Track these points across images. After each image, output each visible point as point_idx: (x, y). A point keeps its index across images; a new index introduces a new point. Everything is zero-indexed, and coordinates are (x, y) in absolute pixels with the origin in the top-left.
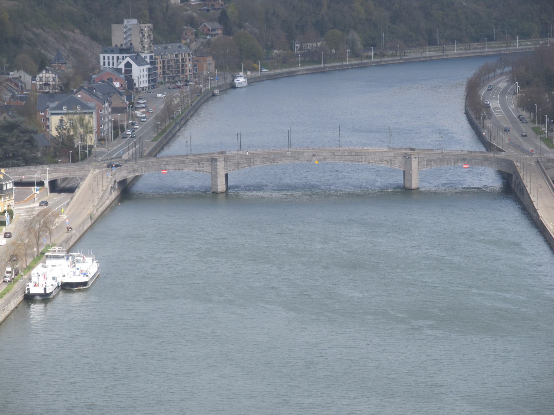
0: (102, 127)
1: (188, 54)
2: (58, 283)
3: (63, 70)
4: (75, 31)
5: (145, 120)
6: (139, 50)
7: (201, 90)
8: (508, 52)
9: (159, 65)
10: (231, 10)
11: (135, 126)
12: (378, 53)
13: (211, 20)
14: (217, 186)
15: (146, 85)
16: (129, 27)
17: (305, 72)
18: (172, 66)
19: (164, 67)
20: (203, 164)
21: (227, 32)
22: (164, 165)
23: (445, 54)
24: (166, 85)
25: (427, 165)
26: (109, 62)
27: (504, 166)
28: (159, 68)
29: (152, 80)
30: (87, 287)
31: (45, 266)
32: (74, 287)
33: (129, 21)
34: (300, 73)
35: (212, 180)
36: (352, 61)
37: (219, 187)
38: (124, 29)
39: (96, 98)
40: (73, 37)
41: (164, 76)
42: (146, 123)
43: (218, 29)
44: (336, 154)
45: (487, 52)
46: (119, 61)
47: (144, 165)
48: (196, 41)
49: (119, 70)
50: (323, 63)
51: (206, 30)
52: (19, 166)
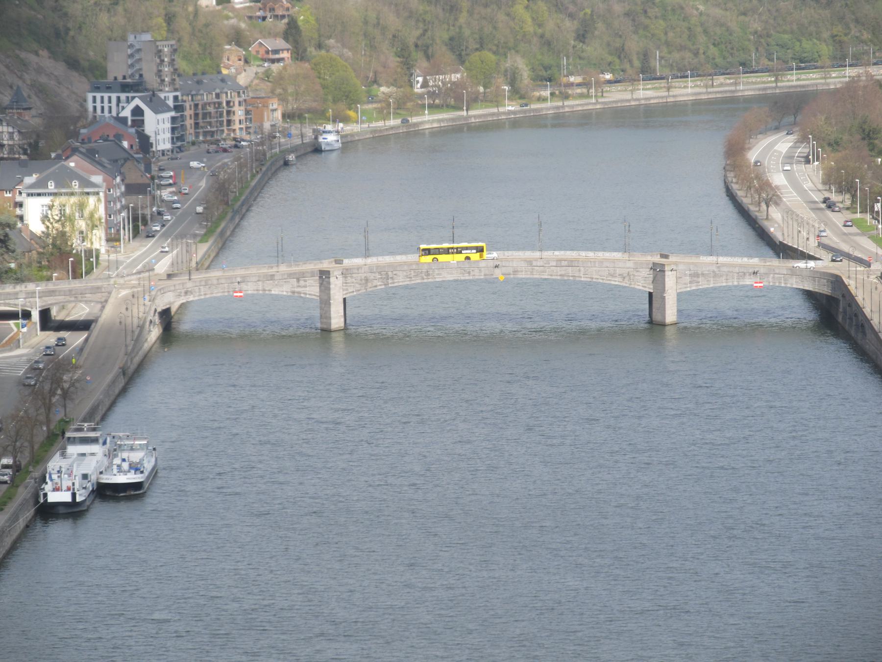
0: (112, 218)
1: (236, 94)
2: (93, 485)
3: (26, 121)
4: (41, 52)
5: (178, 205)
6: (155, 87)
7: (264, 154)
8: (778, 91)
9: (188, 112)
10: (304, 17)
11: (165, 217)
12: (557, 92)
13: (271, 34)
14: (330, 318)
15: (168, 146)
16: (137, 47)
18: (210, 113)
19: (196, 115)
20: (305, 281)
21: (299, 55)
22: (239, 283)
23: (671, 93)
25: (691, 282)
28: (188, 118)
29: (178, 138)
30: (141, 492)
31: (63, 455)
32: (120, 493)
34: (427, 127)
35: (321, 308)
38: (129, 50)
39: (100, 168)
41: (198, 131)
42: (180, 211)
44: (534, 263)
45: (742, 90)
46: (121, 105)
47: (203, 283)
48: (245, 70)
49: (124, 120)
50: (465, 108)
51: (262, 51)
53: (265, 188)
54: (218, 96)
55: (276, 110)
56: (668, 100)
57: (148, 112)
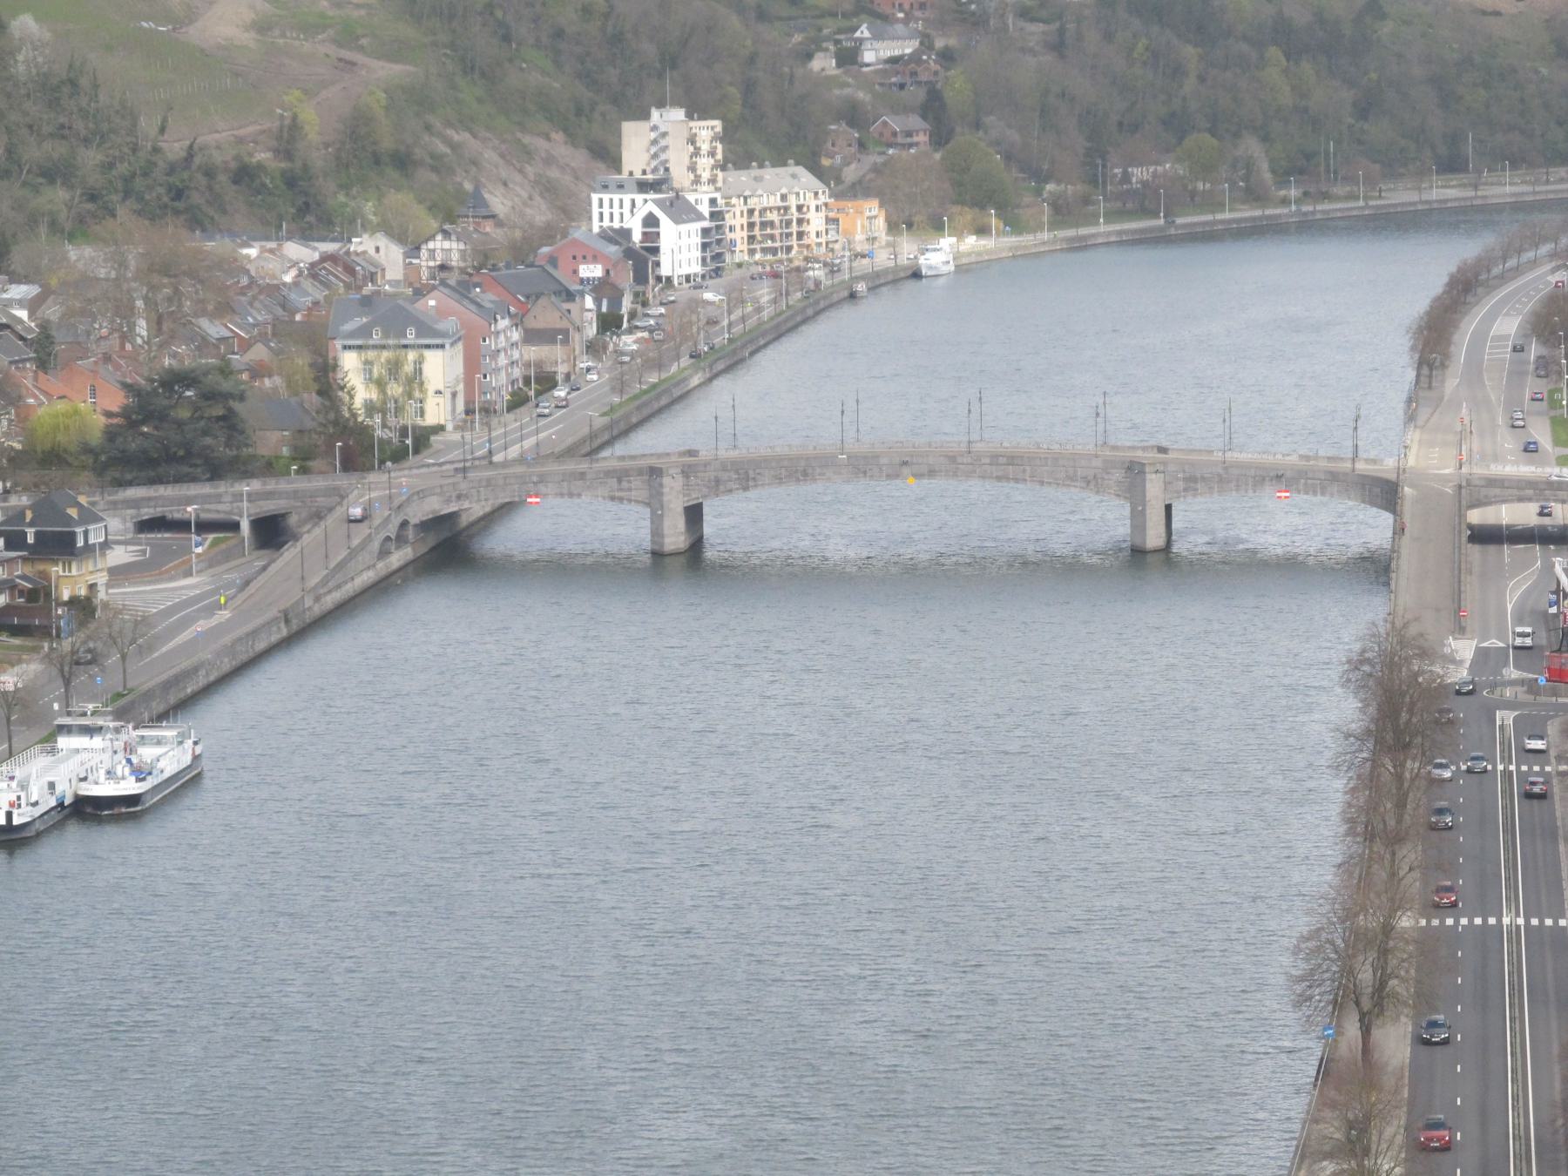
3: (487, 234)
4: (554, 135)
15: (697, 268)
16: (663, 129)
17: (1113, 239)
19: (751, 226)
20: (629, 482)
23: (1479, 193)
24: (751, 268)
25: (1185, 490)
26: (612, 214)
27: (1377, 496)
30: (139, 808)
33: (664, 114)
36: (1245, 210)
37: (667, 540)
38: (652, 134)
40: (546, 151)
41: (752, 247)
43: (917, 132)
44: (959, 460)
47: (484, 484)
50: (1162, 214)
52: (193, 479)
53: (784, 338)
54: (784, 198)
55: (875, 217)
56: (1475, 203)
57: (665, 221)
